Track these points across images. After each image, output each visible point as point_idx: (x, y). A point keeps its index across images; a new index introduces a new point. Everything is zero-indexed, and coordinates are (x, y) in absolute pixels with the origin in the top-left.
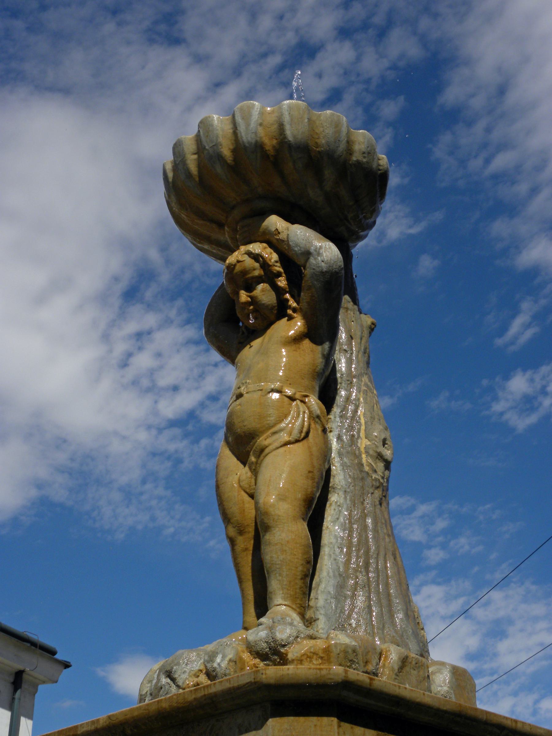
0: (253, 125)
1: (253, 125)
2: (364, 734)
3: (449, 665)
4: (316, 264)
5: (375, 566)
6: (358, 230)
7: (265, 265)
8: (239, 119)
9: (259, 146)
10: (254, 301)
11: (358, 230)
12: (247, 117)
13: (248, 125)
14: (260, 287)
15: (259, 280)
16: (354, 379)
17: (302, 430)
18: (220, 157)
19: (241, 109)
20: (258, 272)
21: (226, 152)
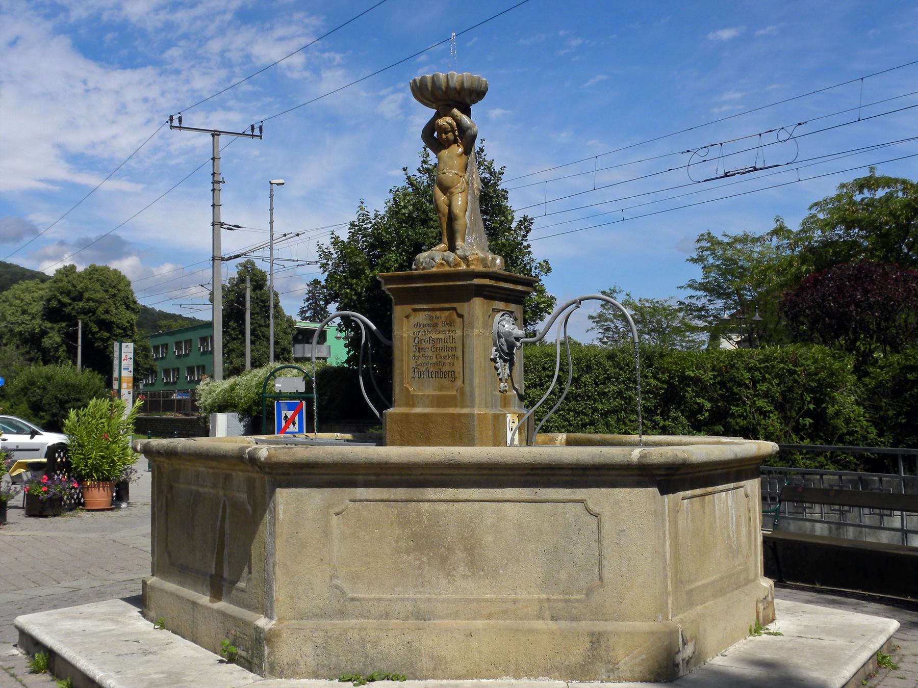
0: (454, 81)
1: (454, 81)
2: (3, 396)
3: (292, 671)
4: (489, 264)
5: (62, 460)
6: (795, 410)
7: (452, 127)
8: (449, 77)
9: (455, 89)
10: (447, 137)
11: (795, 410)
12: (452, 78)
13: (453, 81)
14: (450, 133)
15: (450, 132)
16: (811, 421)
17: (425, 663)
18: (441, 89)
19: (450, 74)
20: (450, 129)
21: (444, 88)
